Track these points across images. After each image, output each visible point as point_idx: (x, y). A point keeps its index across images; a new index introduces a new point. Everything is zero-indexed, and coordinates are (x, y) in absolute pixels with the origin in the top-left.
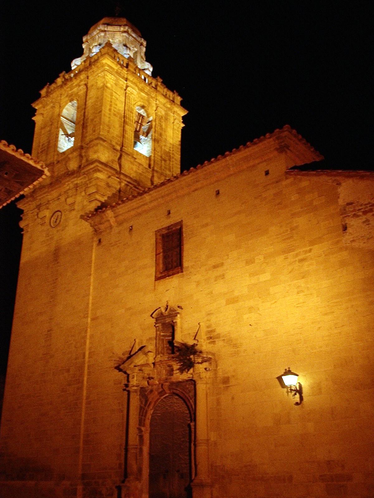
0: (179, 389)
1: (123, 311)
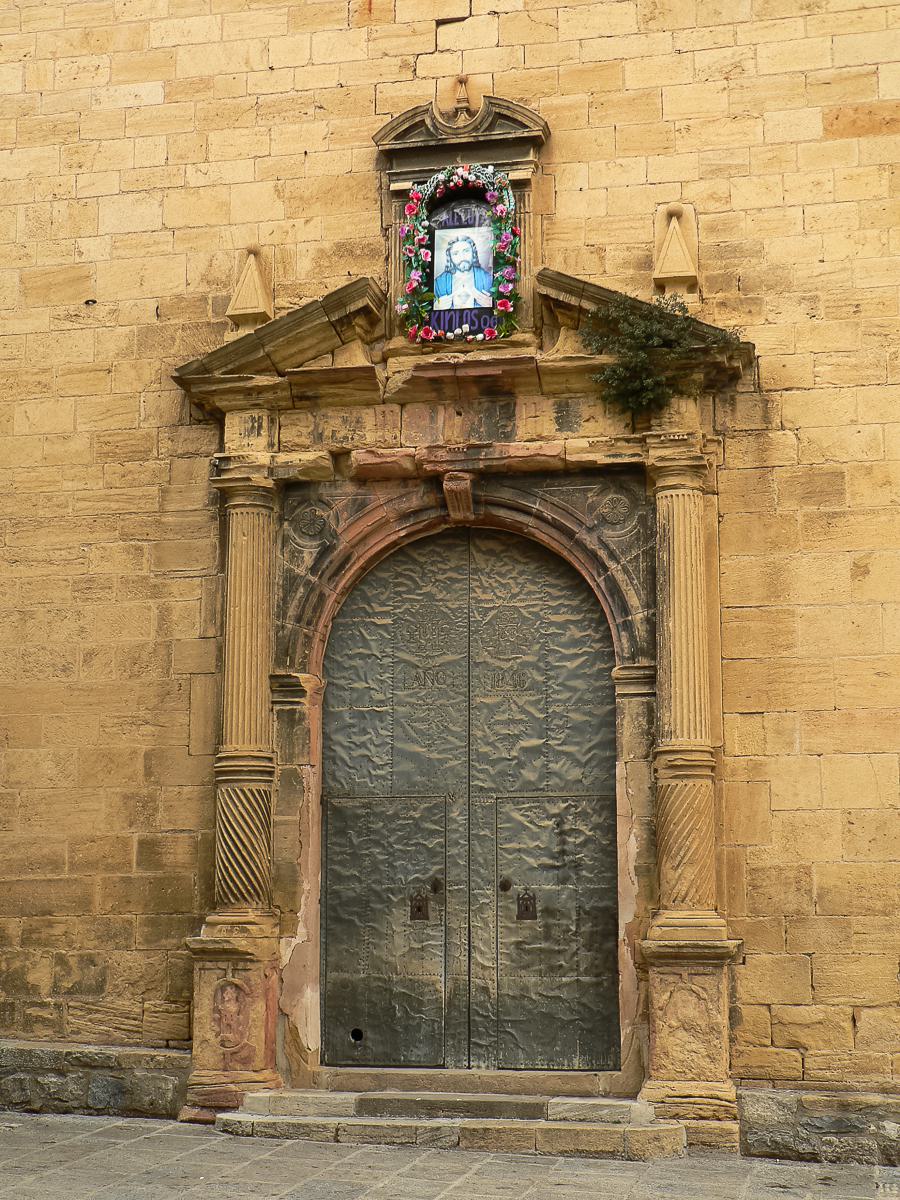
1: (151, 91)
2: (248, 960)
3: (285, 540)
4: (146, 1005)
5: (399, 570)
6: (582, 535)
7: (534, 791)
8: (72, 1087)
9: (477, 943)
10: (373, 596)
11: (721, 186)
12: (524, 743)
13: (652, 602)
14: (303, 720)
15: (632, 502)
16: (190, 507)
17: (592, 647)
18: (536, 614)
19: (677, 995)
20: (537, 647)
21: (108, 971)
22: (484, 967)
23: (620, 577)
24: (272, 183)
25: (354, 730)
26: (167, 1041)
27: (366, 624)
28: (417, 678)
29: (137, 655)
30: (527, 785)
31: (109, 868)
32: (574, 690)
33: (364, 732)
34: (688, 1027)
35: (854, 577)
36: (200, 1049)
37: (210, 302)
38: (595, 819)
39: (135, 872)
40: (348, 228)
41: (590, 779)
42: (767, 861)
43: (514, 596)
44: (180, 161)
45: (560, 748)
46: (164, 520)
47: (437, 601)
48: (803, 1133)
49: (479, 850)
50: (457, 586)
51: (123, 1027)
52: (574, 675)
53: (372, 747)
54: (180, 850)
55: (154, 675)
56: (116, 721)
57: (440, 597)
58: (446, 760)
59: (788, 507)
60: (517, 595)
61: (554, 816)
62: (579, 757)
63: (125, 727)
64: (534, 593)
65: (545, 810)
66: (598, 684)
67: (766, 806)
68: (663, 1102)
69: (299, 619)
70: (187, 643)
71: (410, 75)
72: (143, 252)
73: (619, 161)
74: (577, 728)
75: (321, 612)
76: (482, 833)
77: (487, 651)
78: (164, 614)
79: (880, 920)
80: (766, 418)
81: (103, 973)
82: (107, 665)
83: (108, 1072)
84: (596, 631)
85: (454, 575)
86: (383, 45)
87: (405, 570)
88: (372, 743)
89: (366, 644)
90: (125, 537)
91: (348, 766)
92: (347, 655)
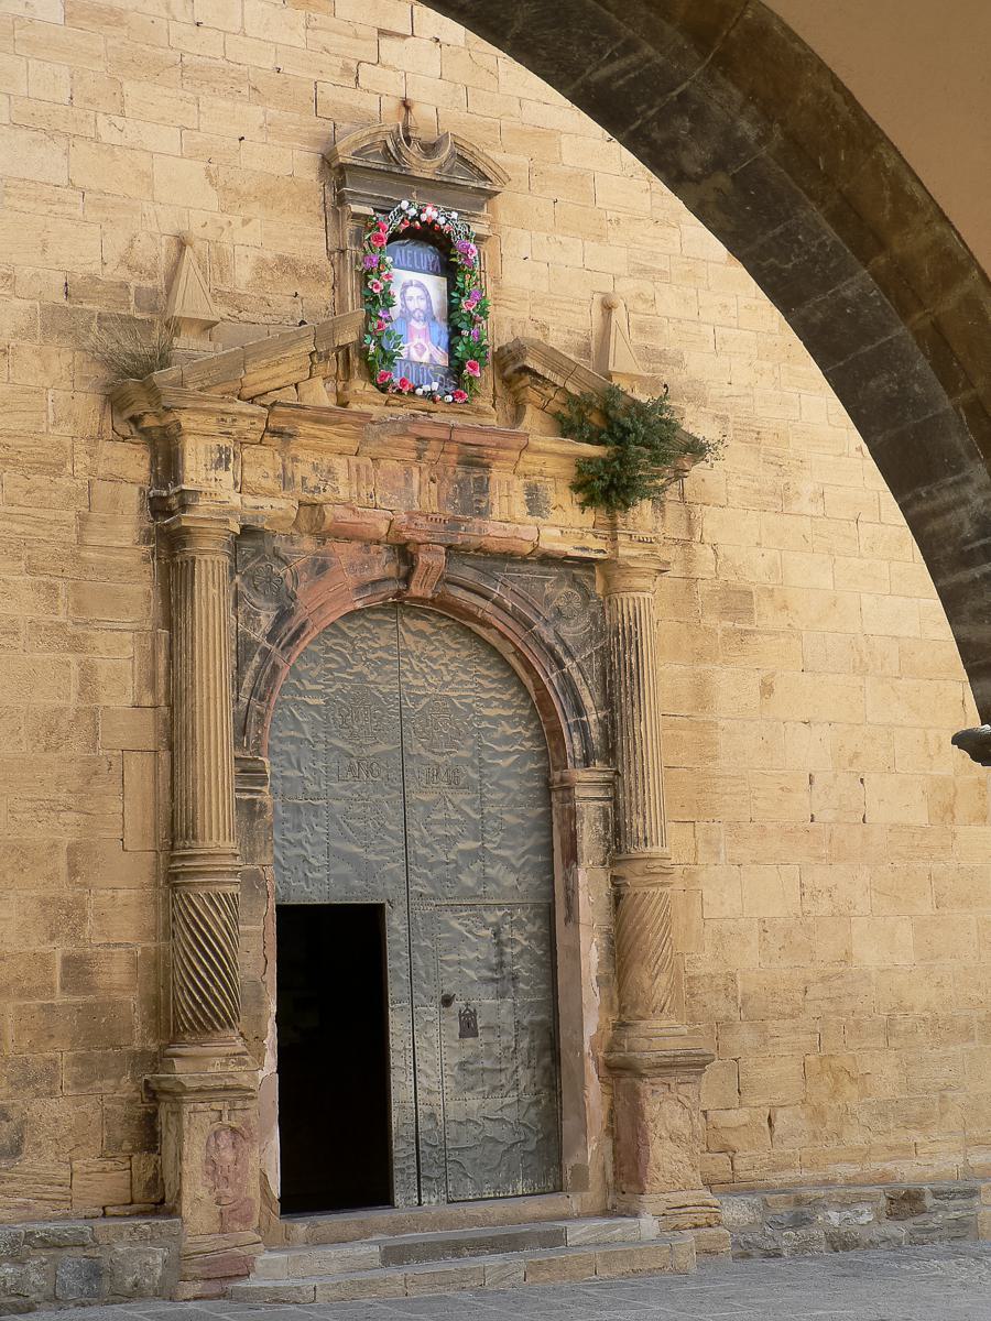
0: (497, 592)
2: (247, 1098)
3: (238, 598)
4: (76, 1165)
5: (329, 644)
6: (538, 626)
7: (471, 897)
8: (34, 1277)
9: (421, 1065)
10: (304, 671)
11: (648, 288)
12: (461, 846)
13: (609, 702)
14: (265, 812)
15: (583, 598)
16: (116, 543)
17: (524, 746)
18: (468, 706)
19: (665, 1105)
20: (470, 742)
21: (27, 1127)
22: (430, 1092)
23: (576, 675)
24: (204, 165)
25: (288, 825)
26: (104, 1208)
27: (297, 703)
28: (351, 769)
29: (53, 722)
30: (467, 892)
31: (23, 994)
32: (508, 790)
33: (299, 828)
34: (674, 1137)
35: (762, 694)
36: (190, 1211)
37: (132, 291)
38: (529, 928)
39: (60, 998)
40: (291, 241)
41: (524, 886)
42: (702, 969)
43: (446, 685)
44: (88, 105)
45: (495, 852)
46: (83, 554)
47: (369, 682)
48: (769, 1231)
49: (420, 962)
50: (388, 667)
51: (46, 1196)
52: (507, 774)
53: (307, 846)
54: (115, 970)
55: (76, 748)
56: (28, 804)
57: (371, 678)
58: (384, 863)
59: (710, 620)
60: (449, 683)
61: (492, 924)
62: (514, 861)
63: (40, 813)
64: (467, 682)
65: (483, 919)
66: (528, 785)
67: (699, 914)
68: (664, 1215)
69: (253, 692)
70: (118, 711)
71: (353, 84)
72: (44, 209)
73: (559, 238)
74: (511, 831)
75: (275, 686)
76: (423, 944)
77: (421, 742)
78: (88, 675)
79: (789, 1023)
80: (690, 530)
81: (20, 1130)
82: (14, 732)
83: (79, 1252)
84: (526, 728)
85: (385, 656)
86: (323, 37)
87: (336, 644)
88: (308, 842)
89: (298, 725)
90: (32, 570)
91: (282, 866)
92: (277, 737)
